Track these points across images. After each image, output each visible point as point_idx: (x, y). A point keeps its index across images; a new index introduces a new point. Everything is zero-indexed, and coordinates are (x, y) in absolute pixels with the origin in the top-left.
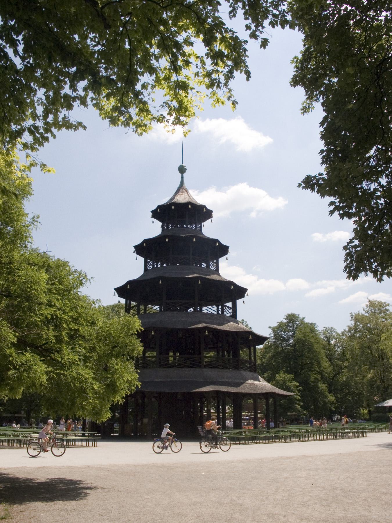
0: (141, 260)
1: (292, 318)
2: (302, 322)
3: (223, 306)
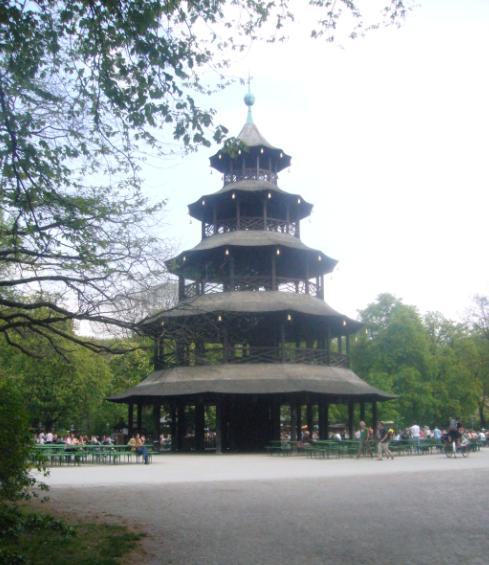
0: (198, 224)
1: (385, 300)
2: (399, 305)
3: (307, 284)
